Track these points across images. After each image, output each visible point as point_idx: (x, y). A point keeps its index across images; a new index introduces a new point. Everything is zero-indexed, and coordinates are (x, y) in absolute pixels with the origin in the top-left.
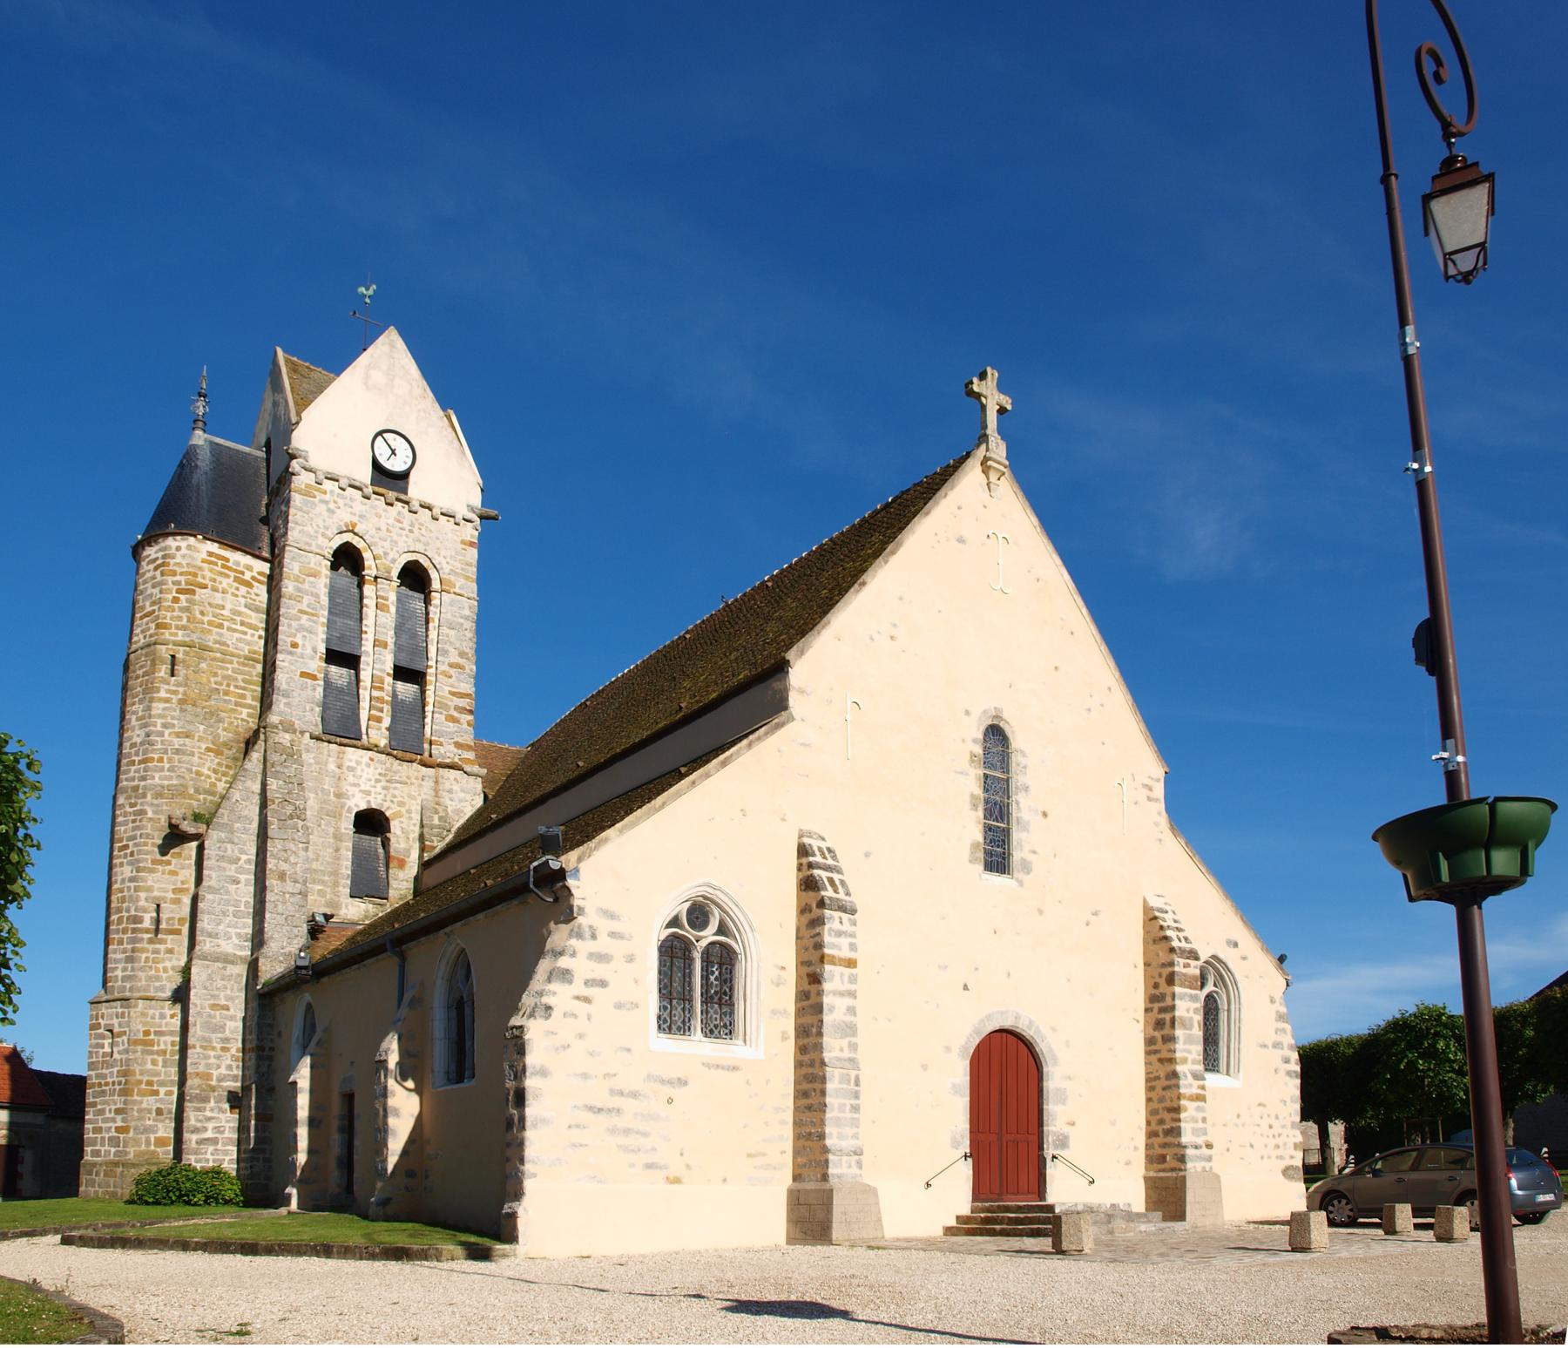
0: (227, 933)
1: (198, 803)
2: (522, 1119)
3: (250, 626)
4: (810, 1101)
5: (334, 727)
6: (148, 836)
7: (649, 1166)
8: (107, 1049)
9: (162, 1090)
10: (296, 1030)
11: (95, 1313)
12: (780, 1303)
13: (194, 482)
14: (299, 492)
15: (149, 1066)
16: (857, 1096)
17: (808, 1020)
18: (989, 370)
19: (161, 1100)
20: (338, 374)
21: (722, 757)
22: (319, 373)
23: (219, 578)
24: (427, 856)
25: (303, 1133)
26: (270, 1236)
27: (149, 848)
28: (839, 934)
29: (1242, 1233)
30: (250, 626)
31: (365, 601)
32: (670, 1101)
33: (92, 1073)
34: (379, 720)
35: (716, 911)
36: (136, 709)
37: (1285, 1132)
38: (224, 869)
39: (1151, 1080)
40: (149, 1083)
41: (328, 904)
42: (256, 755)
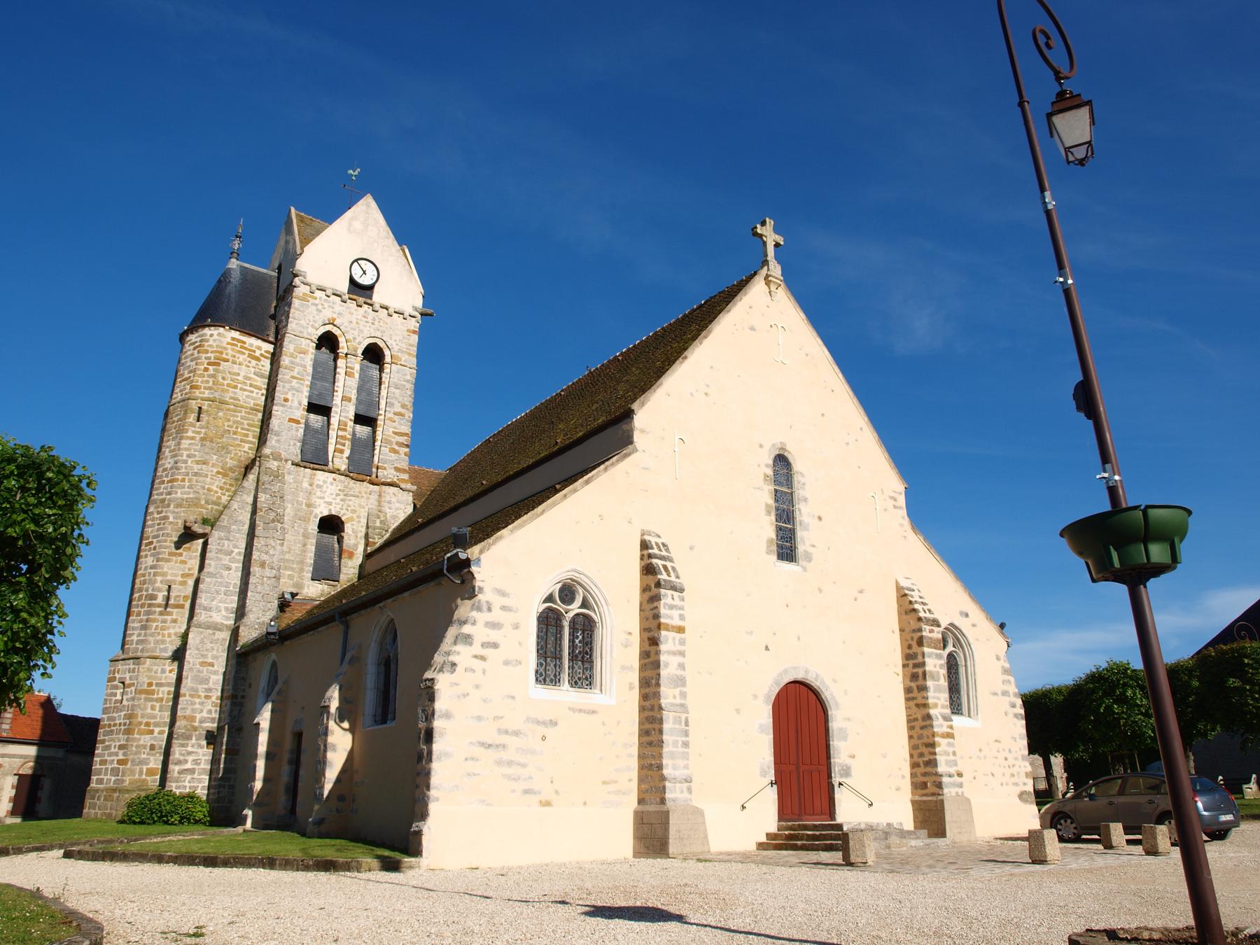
0: (218, 608)
2: (430, 753)
5: (309, 457)
6: (168, 535)
7: (526, 792)
8: (119, 697)
9: (157, 730)
10: (263, 683)
12: (628, 908)
15: (149, 711)
16: (687, 735)
17: (649, 673)
21: (586, 478)
22: (318, 223)
24: (369, 550)
25: (261, 765)
26: (227, 851)
28: (672, 607)
32: (544, 738)
33: (105, 716)
34: (342, 452)
35: (580, 590)
36: (170, 444)
39: (911, 721)
40: (148, 724)
41: (297, 585)
42: (252, 477)
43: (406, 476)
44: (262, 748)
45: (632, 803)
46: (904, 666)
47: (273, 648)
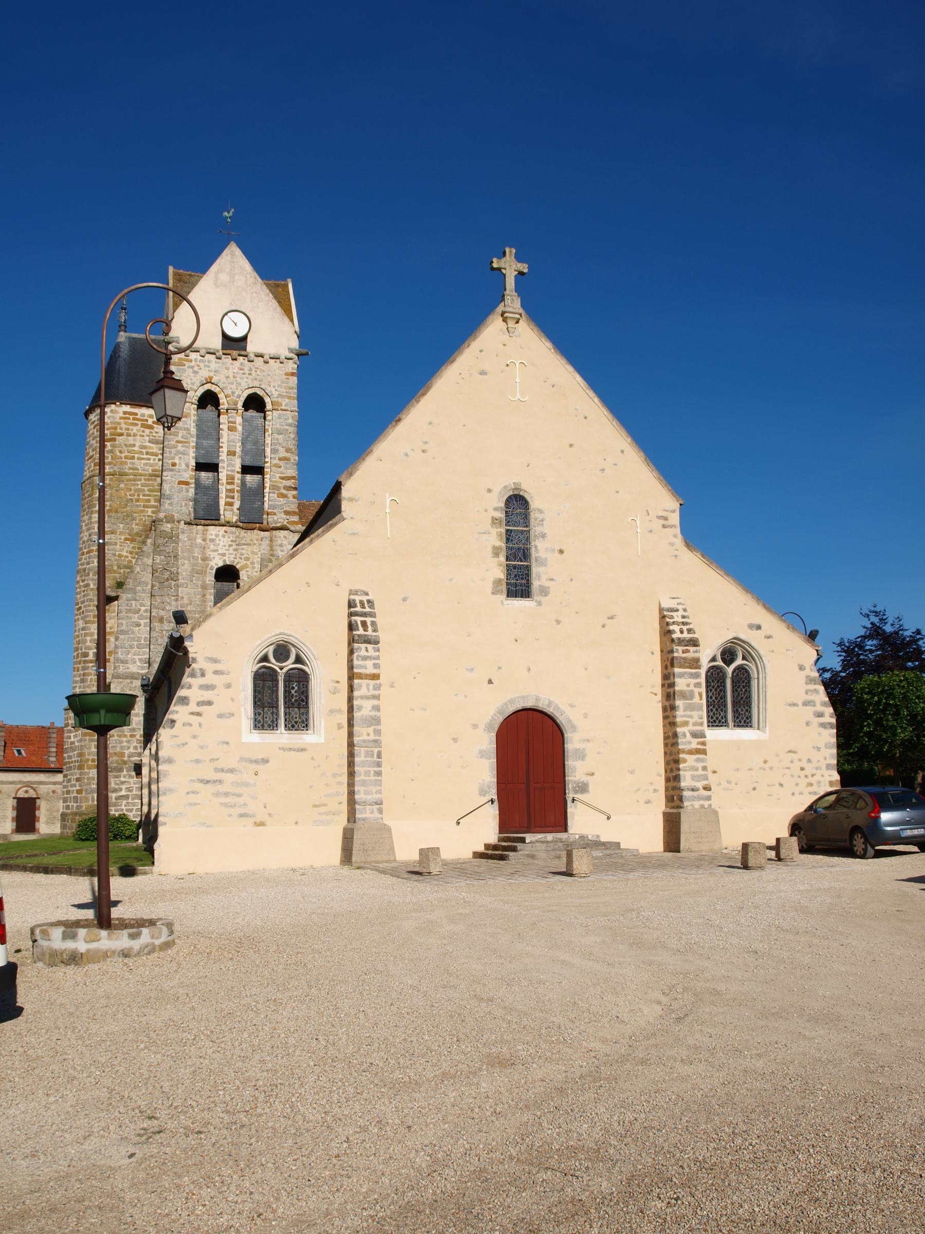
6: (91, 600)
7: (242, 815)
13: (117, 367)
14: (175, 365)
16: (379, 765)
18: (507, 250)
23: (131, 427)
27: (92, 608)
28: (365, 658)
34: (231, 504)
37: (819, 773)
38: (131, 618)
43: (295, 518)
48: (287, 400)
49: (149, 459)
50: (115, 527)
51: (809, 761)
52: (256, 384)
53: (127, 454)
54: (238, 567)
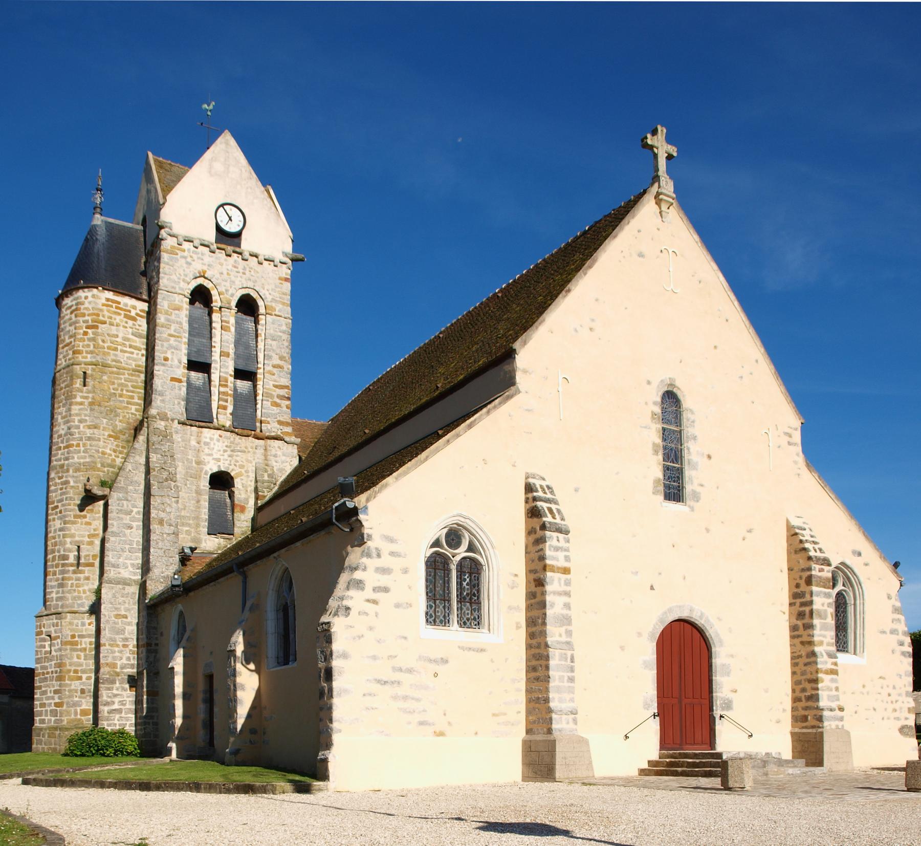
0: (124, 564)
1: (104, 473)
2: (331, 690)
3: (136, 348)
4: (538, 674)
5: (194, 415)
6: (71, 499)
7: (421, 723)
8: (48, 649)
9: (84, 676)
10: (173, 631)
11: (46, 831)
12: (519, 824)
13: (96, 250)
14: (167, 252)
15: (75, 659)
16: (572, 670)
17: (535, 613)
18: (659, 128)
19: (83, 684)
20: (190, 167)
21: (468, 422)
22: (177, 168)
23: (113, 316)
24: (260, 503)
25: (179, 704)
26: (158, 777)
27: (72, 507)
28: (557, 549)
29: (868, 777)
30: (136, 348)
31: (214, 325)
32: (436, 675)
33: (38, 666)
34: (225, 408)
35: (466, 534)
36: (61, 410)
38: (122, 519)
39: (795, 658)
40: (76, 671)
41: (194, 540)
42: (142, 438)
44: (179, 688)
45: (520, 733)
46: (790, 604)
47: (178, 600)
48: (281, 306)
49: (132, 353)
50: (98, 421)
51: (894, 688)
52: (250, 284)
53: (109, 344)
54: (232, 474)
